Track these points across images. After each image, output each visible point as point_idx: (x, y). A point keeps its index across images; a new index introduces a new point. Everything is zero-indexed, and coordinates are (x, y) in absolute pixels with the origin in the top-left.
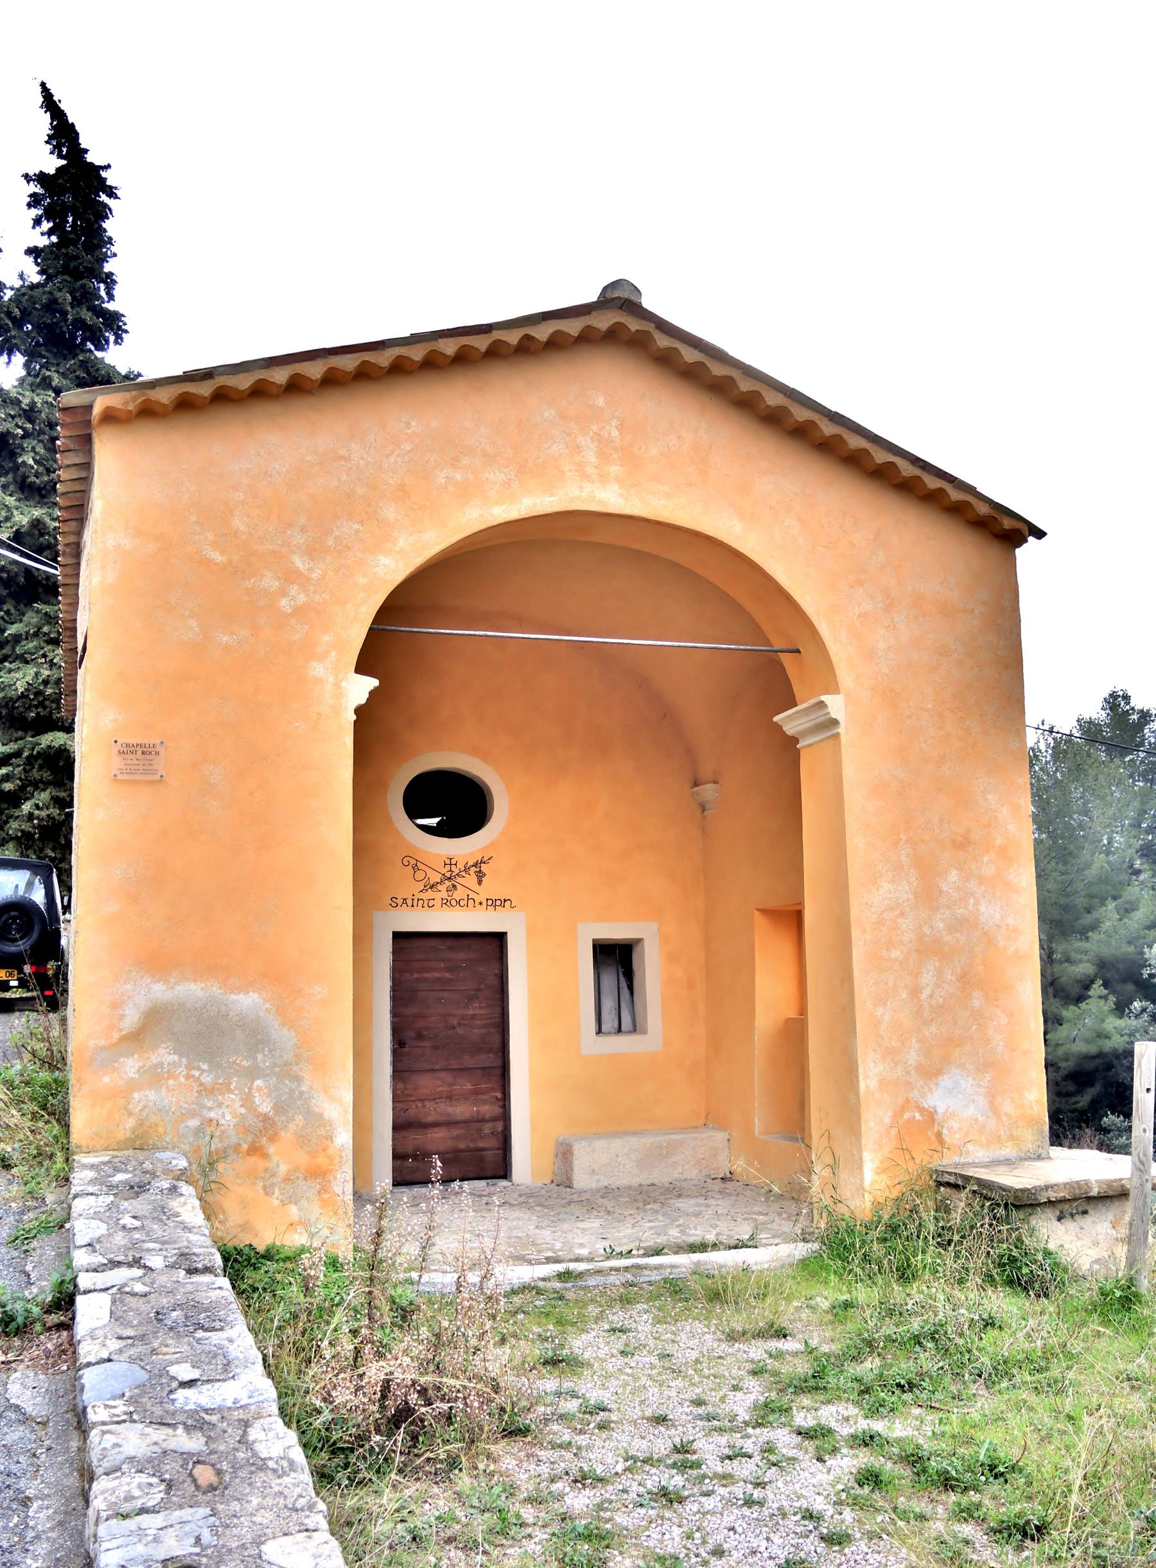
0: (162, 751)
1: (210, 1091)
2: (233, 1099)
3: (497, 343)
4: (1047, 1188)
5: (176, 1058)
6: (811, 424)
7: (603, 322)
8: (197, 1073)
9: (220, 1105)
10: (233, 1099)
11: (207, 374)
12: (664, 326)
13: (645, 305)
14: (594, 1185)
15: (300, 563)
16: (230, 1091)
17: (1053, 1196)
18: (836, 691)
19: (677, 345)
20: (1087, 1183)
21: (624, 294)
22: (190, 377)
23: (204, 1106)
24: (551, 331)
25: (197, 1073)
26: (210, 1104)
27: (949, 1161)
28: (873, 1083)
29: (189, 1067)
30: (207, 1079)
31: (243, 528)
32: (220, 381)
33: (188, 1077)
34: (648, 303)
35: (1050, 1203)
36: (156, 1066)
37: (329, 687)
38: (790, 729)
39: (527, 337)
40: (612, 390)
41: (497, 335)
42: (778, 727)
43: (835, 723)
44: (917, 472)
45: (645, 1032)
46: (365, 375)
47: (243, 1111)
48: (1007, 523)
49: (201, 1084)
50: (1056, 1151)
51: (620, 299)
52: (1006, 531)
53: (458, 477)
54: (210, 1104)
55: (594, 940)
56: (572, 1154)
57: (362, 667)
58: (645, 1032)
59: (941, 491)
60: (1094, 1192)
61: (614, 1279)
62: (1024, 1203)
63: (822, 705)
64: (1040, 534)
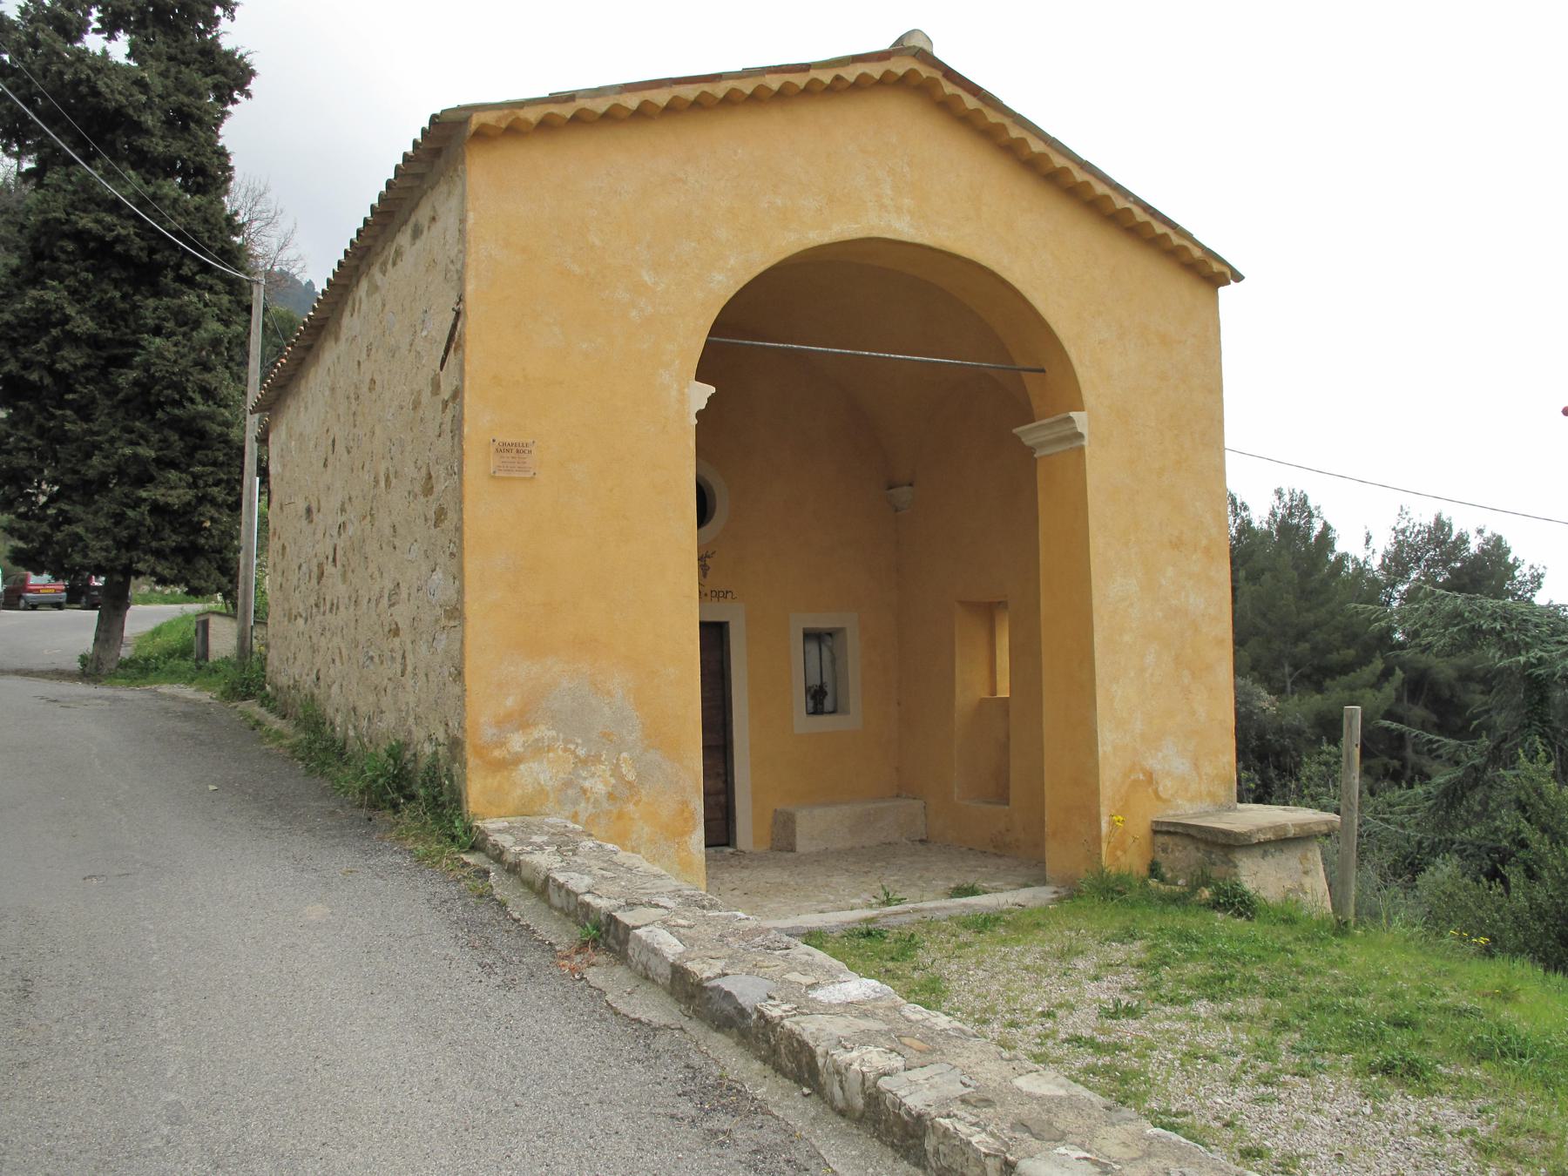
0: (533, 448)
1: (583, 762)
2: (603, 769)
3: (814, 81)
4: (1259, 830)
5: (554, 733)
6: (1066, 171)
7: (900, 67)
8: (572, 747)
9: (593, 775)
10: (603, 769)
11: (570, 97)
12: (950, 74)
13: (936, 54)
14: (813, 849)
15: (647, 277)
16: (601, 762)
17: (1262, 837)
18: (1081, 409)
19: (959, 92)
20: (1285, 825)
21: (921, 44)
22: (555, 99)
23: (579, 776)
24: (858, 73)
25: (572, 747)
26: (584, 774)
27: (1168, 815)
28: (1109, 749)
29: (566, 741)
30: (581, 752)
31: (597, 242)
32: (581, 103)
33: (566, 750)
34: (940, 53)
35: (1260, 844)
36: (537, 740)
37: (674, 393)
38: (1028, 441)
39: (838, 78)
40: (905, 127)
41: (813, 74)
42: (1017, 438)
43: (1080, 436)
44: (1147, 218)
45: (846, 712)
46: (701, 105)
47: (613, 781)
48: (1216, 267)
49: (577, 757)
50: (1240, 806)
51: (912, 49)
52: (1209, 273)
53: (779, 202)
54: (584, 774)
55: (727, 623)
56: (794, 822)
57: (701, 376)
58: (846, 712)
59: (1165, 236)
60: (1291, 833)
61: (907, 919)
62: (1227, 845)
63: (1070, 420)
64: (1238, 277)
